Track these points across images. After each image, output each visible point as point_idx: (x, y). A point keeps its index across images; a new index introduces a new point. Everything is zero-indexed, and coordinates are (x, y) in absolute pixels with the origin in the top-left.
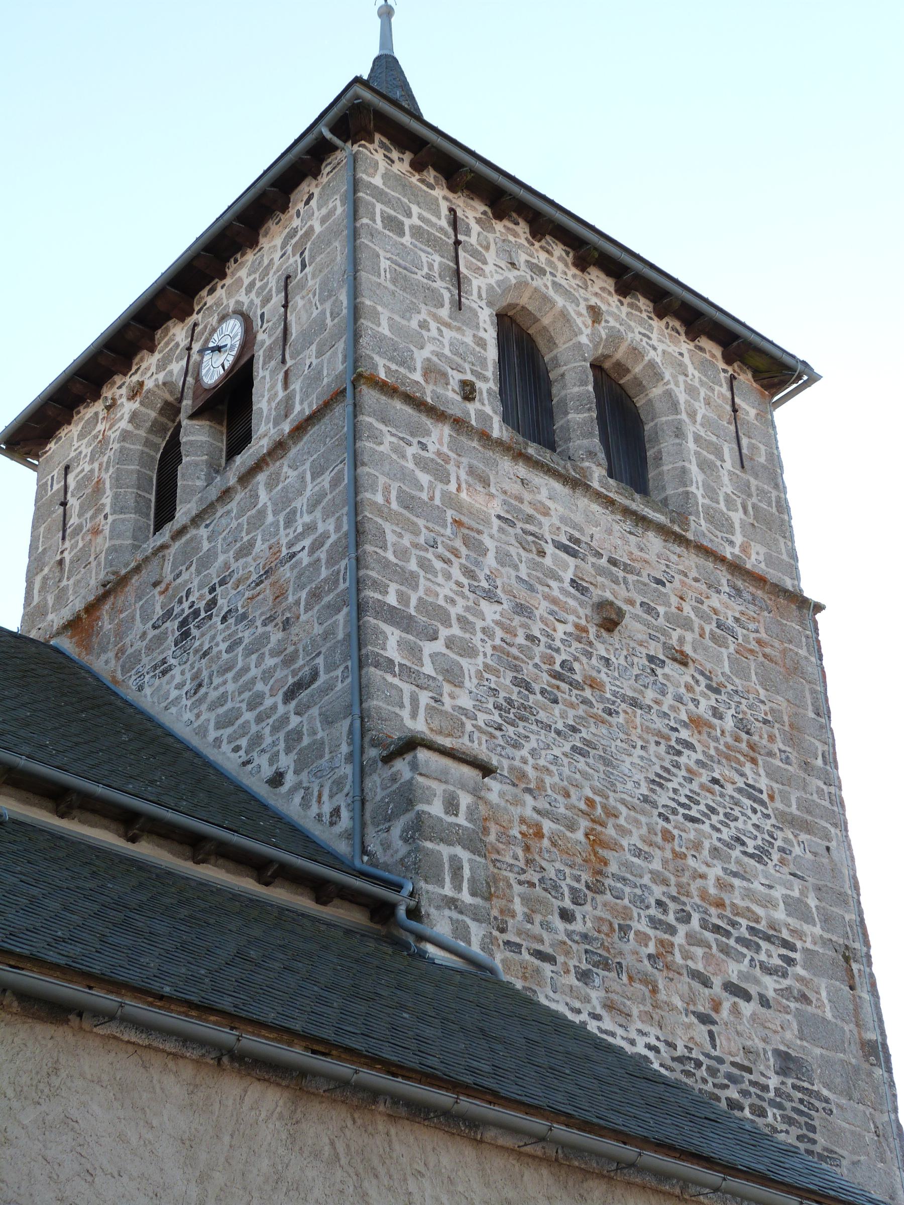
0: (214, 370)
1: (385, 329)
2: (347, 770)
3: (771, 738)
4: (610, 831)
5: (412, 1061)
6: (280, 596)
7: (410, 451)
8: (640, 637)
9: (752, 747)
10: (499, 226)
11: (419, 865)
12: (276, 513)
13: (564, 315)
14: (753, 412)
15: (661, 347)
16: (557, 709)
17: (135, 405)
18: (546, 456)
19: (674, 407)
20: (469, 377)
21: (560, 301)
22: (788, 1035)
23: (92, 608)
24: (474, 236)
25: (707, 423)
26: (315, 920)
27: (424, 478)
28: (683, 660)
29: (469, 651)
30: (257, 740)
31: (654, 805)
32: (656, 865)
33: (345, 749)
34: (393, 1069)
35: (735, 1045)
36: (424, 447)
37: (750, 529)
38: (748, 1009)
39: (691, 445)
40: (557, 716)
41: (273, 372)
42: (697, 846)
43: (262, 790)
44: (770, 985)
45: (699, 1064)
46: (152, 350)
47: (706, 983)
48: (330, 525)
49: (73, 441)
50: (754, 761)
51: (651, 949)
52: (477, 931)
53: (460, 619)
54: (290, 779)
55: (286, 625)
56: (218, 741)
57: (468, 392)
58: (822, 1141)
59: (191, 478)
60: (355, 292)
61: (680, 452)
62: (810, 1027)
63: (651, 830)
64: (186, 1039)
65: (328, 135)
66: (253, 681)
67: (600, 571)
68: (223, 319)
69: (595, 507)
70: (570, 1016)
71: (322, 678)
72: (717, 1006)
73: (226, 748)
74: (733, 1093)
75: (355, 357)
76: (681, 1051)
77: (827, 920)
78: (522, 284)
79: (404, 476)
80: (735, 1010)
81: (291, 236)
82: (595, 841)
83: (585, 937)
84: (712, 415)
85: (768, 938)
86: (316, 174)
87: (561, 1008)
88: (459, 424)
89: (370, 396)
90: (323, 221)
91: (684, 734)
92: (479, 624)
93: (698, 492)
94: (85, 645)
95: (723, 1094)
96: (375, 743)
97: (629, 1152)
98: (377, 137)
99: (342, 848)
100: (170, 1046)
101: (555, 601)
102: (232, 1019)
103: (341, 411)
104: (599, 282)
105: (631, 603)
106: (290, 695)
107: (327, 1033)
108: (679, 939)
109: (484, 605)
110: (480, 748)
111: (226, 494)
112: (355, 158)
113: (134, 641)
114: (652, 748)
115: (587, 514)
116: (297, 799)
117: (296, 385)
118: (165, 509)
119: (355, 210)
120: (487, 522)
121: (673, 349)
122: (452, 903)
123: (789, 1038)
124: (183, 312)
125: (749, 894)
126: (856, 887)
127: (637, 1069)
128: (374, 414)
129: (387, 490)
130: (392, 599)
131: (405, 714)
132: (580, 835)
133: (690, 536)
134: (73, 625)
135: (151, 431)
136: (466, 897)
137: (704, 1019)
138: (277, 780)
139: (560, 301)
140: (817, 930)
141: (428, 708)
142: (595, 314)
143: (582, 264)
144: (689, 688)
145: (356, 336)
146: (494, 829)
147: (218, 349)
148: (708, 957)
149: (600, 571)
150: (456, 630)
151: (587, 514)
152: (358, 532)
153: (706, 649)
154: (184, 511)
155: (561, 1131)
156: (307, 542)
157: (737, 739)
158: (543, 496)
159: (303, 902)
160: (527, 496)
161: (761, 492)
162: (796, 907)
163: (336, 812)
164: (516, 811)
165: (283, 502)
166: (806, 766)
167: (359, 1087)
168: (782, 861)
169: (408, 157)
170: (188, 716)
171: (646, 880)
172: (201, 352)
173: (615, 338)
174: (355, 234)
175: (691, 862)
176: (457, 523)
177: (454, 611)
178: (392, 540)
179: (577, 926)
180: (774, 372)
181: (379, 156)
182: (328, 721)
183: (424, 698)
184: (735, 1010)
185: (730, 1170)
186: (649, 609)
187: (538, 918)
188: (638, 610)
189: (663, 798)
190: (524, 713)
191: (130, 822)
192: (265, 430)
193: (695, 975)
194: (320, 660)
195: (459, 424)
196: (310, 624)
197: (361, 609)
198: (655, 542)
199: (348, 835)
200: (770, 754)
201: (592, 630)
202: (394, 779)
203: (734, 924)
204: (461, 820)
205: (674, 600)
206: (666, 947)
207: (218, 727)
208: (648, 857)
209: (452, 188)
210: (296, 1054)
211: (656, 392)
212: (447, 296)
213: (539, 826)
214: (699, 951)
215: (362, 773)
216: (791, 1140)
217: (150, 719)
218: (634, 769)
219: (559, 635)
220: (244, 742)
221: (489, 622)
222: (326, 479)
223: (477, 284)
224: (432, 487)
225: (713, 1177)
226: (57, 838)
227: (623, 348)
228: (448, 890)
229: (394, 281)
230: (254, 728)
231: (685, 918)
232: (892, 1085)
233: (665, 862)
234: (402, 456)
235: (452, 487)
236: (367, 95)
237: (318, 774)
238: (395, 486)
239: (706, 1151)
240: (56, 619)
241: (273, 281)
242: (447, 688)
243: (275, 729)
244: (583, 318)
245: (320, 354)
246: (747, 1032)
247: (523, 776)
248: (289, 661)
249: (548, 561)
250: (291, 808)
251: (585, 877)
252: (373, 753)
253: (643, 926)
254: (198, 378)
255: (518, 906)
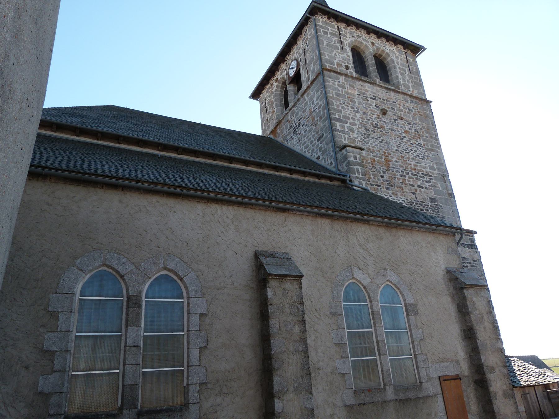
0: (292, 73)
1: (327, 57)
2: (332, 154)
3: (423, 132)
4: (390, 158)
5: (354, 211)
6: (313, 119)
7: (336, 83)
8: (392, 115)
9: (419, 135)
10: (349, 28)
11: (350, 171)
12: (309, 102)
13: (366, 46)
14: (411, 60)
15: (389, 49)
16: (375, 134)
17: (277, 83)
18: (366, 79)
19: (393, 62)
20: (347, 64)
21: (365, 43)
22: (432, 194)
23: (275, 128)
24: (344, 31)
25: (401, 64)
26: (330, 185)
27: (340, 89)
28: (401, 119)
29: (355, 125)
30: (313, 150)
31: (398, 151)
32: (400, 163)
33: (331, 149)
34: (350, 213)
35: (421, 198)
36: (339, 82)
37: (414, 87)
38: (423, 190)
39: (398, 70)
40: (375, 135)
41: (305, 71)
42: (409, 158)
43: (315, 160)
44: (427, 185)
45: (413, 203)
46: (278, 71)
47: (413, 186)
48: (322, 103)
49: (265, 94)
50: (419, 138)
51: (401, 181)
52: (364, 183)
53: (352, 118)
54: (321, 157)
55: (316, 125)
56: (305, 152)
57: (347, 67)
58: (441, 214)
59: (291, 97)
60: (319, 50)
61: (396, 72)
62: (437, 192)
63: (399, 156)
64: (309, 212)
65: (308, 15)
66: (310, 138)
67: (381, 102)
68: (292, 61)
69: (378, 88)
70: (386, 197)
71: (325, 135)
72: (416, 191)
73: (307, 153)
74: (421, 207)
75: (321, 65)
76: (409, 200)
77: (439, 170)
78: (356, 41)
79: (335, 89)
80: (420, 191)
81: (304, 40)
82: (387, 160)
83: (387, 180)
84: (402, 62)
85: (426, 175)
86: (307, 25)
87: (383, 196)
88: (346, 75)
89: (326, 73)
90: (310, 35)
91: (404, 135)
92: (356, 118)
93: (401, 81)
94: (275, 136)
95: (419, 208)
96: (337, 147)
97: (400, 222)
98: (319, 13)
99: (334, 170)
100: (306, 214)
101: (372, 111)
102: (317, 207)
103: (320, 77)
104: (373, 36)
105: (389, 108)
106: (319, 140)
107: (336, 208)
108: (407, 178)
109: (357, 114)
110: (360, 145)
111: (299, 100)
112: (315, 19)
113: (285, 134)
114: (397, 139)
115: (376, 90)
116: (323, 161)
117: (310, 73)
118: (287, 105)
119: (317, 31)
120: (355, 96)
121: (391, 49)
122: (358, 178)
123: (432, 194)
124: (283, 61)
125: (421, 166)
126: (445, 162)
127: (400, 206)
128: (327, 77)
129: (332, 93)
130: (337, 116)
131: (343, 140)
132: (383, 160)
133: (400, 91)
134: (272, 132)
135: (281, 88)
136: (361, 176)
137: (414, 194)
138: (318, 158)
139: (365, 43)
140: (437, 172)
141: (348, 138)
142: (373, 44)
143: (368, 33)
144: (403, 125)
145: (321, 60)
146: (365, 161)
147: (292, 68)
148: (413, 181)
149: (381, 102)
150: (351, 121)
151: (376, 90)
152: (328, 103)
153: (406, 115)
154: (291, 105)
155: (385, 220)
156: (317, 107)
157: (415, 134)
158: (366, 88)
159: (328, 182)
160: (363, 89)
161: (415, 78)
162: (432, 168)
163: (331, 163)
164: (369, 157)
165: (311, 99)
166: (431, 137)
167: (344, 217)
168: (428, 159)
169: (326, 16)
170: (298, 147)
171: (398, 167)
172: (289, 69)
173: (378, 49)
174: (317, 37)
175: (408, 162)
176: (349, 97)
177: (350, 117)
178: (335, 104)
179: (385, 179)
180: (415, 49)
181: (320, 18)
182: (327, 144)
183: (347, 136)
184: (420, 191)
185: (421, 223)
186: (393, 109)
187: (376, 178)
188: (390, 109)
189: (400, 149)
190: (368, 136)
191: (291, 171)
192: (305, 85)
193: (411, 185)
194: (324, 132)
195: (346, 75)
196: (320, 124)
197: (331, 120)
198: (392, 93)
199: (335, 167)
200: (423, 136)
201: (381, 116)
202: (342, 154)
203: (418, 173)
204: (358, 160)
205: (398, 106)
206: (404, 180)
207: (305, 148)
208: (398, 162)
209: (337, 22)
210: (331, 212)
211: (389, 59)
212: (339, 47)
213: (374, 159)
214: (411, 180)
215: (336, 154)
216: (434, 215)
217: (291, 149)
218: (393, 145)
219: (374, 118)
220: (310, 151)
221: (358, 118)
222: (319, 92)
223: (346, 42)
224: (342, 90)
225: (418, 225)
226: (277, 176)
227: (380, 51)
228: (357, 175)
229: (327, 46)
230: (312, 148)
231: (408, 174)
232: (455, 201)
233: (402, 163)
234: (334, 84)
235: (346, 90)
236: (315, 4)
237: (327, 155)
238: (334, 92)
239: (416, 220)
240: (268, 131)
241: (301, 51)
242: (351, 133)
243: (316, 147)
244: (371, 45)
245: (314, 65)
246: (423, 195)
247: (370, 149)
248: (317, 133)
249: (369, 102)
250: (322, 163)
251: (385, 168)
252: (337, 149)
253: (399, 177)
254: (289, 75)
255: (372, 176)
